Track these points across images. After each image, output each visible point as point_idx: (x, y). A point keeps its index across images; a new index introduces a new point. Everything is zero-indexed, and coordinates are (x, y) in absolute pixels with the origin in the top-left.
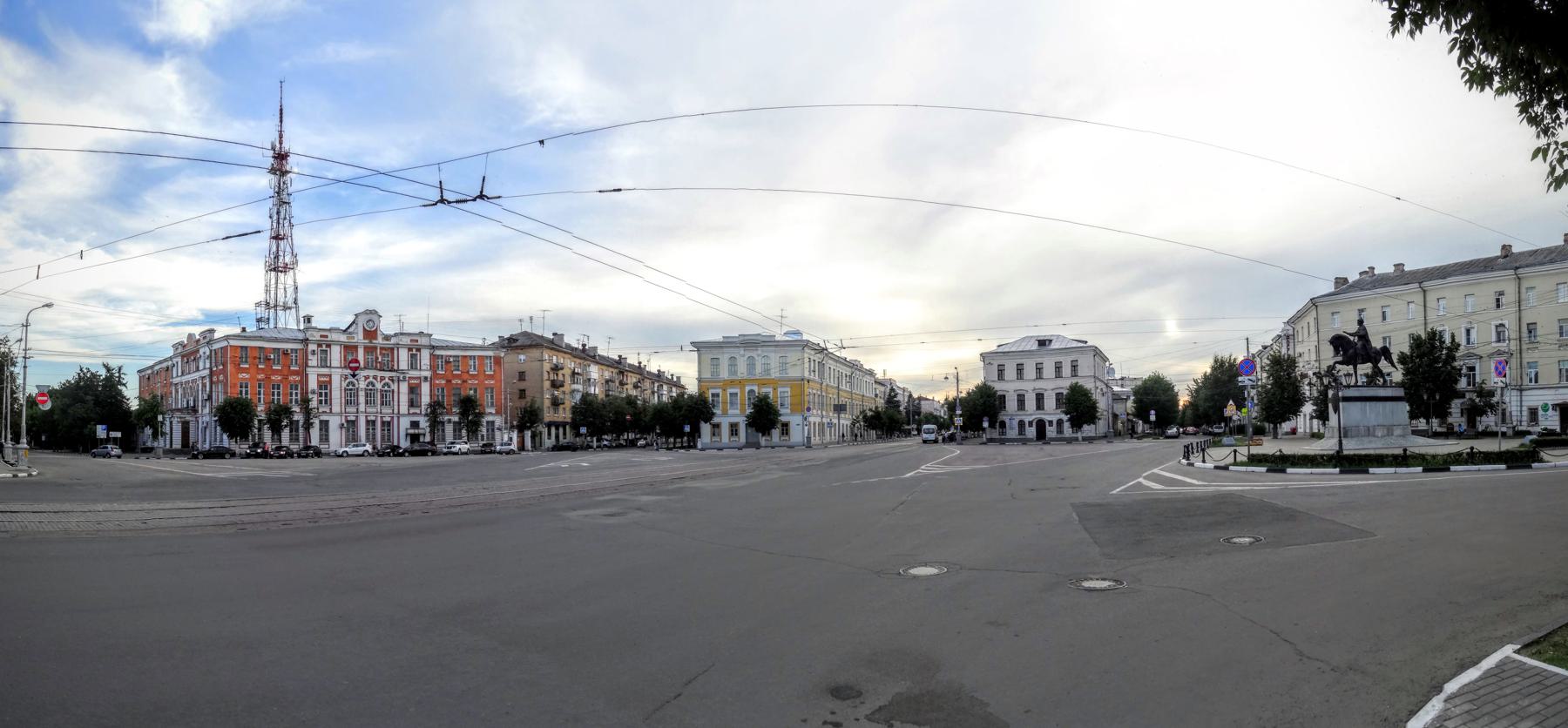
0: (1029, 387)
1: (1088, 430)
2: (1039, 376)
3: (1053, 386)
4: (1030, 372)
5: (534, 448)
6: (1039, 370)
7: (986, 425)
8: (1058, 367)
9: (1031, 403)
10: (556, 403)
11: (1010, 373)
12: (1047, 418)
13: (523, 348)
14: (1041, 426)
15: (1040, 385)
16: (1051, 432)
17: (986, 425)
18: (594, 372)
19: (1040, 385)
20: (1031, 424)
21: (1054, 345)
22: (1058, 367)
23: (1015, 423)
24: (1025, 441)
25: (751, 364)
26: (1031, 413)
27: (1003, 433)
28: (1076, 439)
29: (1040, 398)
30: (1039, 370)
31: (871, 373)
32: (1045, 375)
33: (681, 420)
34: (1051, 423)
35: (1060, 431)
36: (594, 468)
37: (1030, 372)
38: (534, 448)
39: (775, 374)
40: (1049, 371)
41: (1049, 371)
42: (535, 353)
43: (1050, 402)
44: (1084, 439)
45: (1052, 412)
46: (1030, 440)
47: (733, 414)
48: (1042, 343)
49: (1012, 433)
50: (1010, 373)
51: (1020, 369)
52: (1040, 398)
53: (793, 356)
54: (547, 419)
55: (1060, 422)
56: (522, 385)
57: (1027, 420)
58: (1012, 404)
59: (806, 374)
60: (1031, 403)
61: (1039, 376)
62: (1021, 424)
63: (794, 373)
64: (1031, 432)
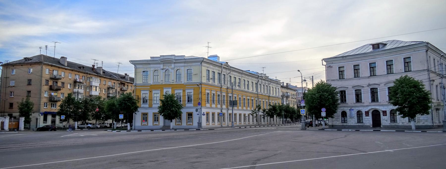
0: (365, 83)
1: (422, 119)
2: (373, 73)
3: (384, 82)
4: (365, 71)
5: (27, 128)
6: (372, 68)
7: (323, 114)
8: (389, 65)
9: (366, 96)
10: (52, 101)
11: (349, 73)
12: (381, 109)
13: (31, 64)
14: (376, 115)
15: (373, 81)
16: (385, 120)
17: (323, 114)
18: (96, 82)
19: (373, 81)
20: (367, 113)
21: (387, 47)
22: (389, 65)
23: (354, 113)
24: (357, 129)
25: (189, 75)
26: (367, 104)
27: (345, 121)
28: (409, 128)
29: (374, 93)
30: (372, 68)
31: (277, 82)
32: (377, 73)
33: (121, 109)
34: (385, 113)
35: (393, 120)
36: (99, 136)
37: (365, 71)
38: (27, 128)
39: (184, 80)
40: (381, 69)
41: (381, 69)
42: (38, 67)
43: (383, 95)
44: (418, 128)
45: (384, 104)
46: (367, 127)
47: (151, 106)
48: (376, 46)
49: (352, 121)
50: (349, 73)
51: (356, 69)
52: (374, 93)
53: (195, 69)
54: (44, 109)
55: (393, 113)
56: (29, 88)
57: (364, 110)
58: (351, 97)
59: (204, 80)
60: (366, 96)
61: (373, 73)
62: (359, 114)
63: (195, 80)
64: (368, 120)
